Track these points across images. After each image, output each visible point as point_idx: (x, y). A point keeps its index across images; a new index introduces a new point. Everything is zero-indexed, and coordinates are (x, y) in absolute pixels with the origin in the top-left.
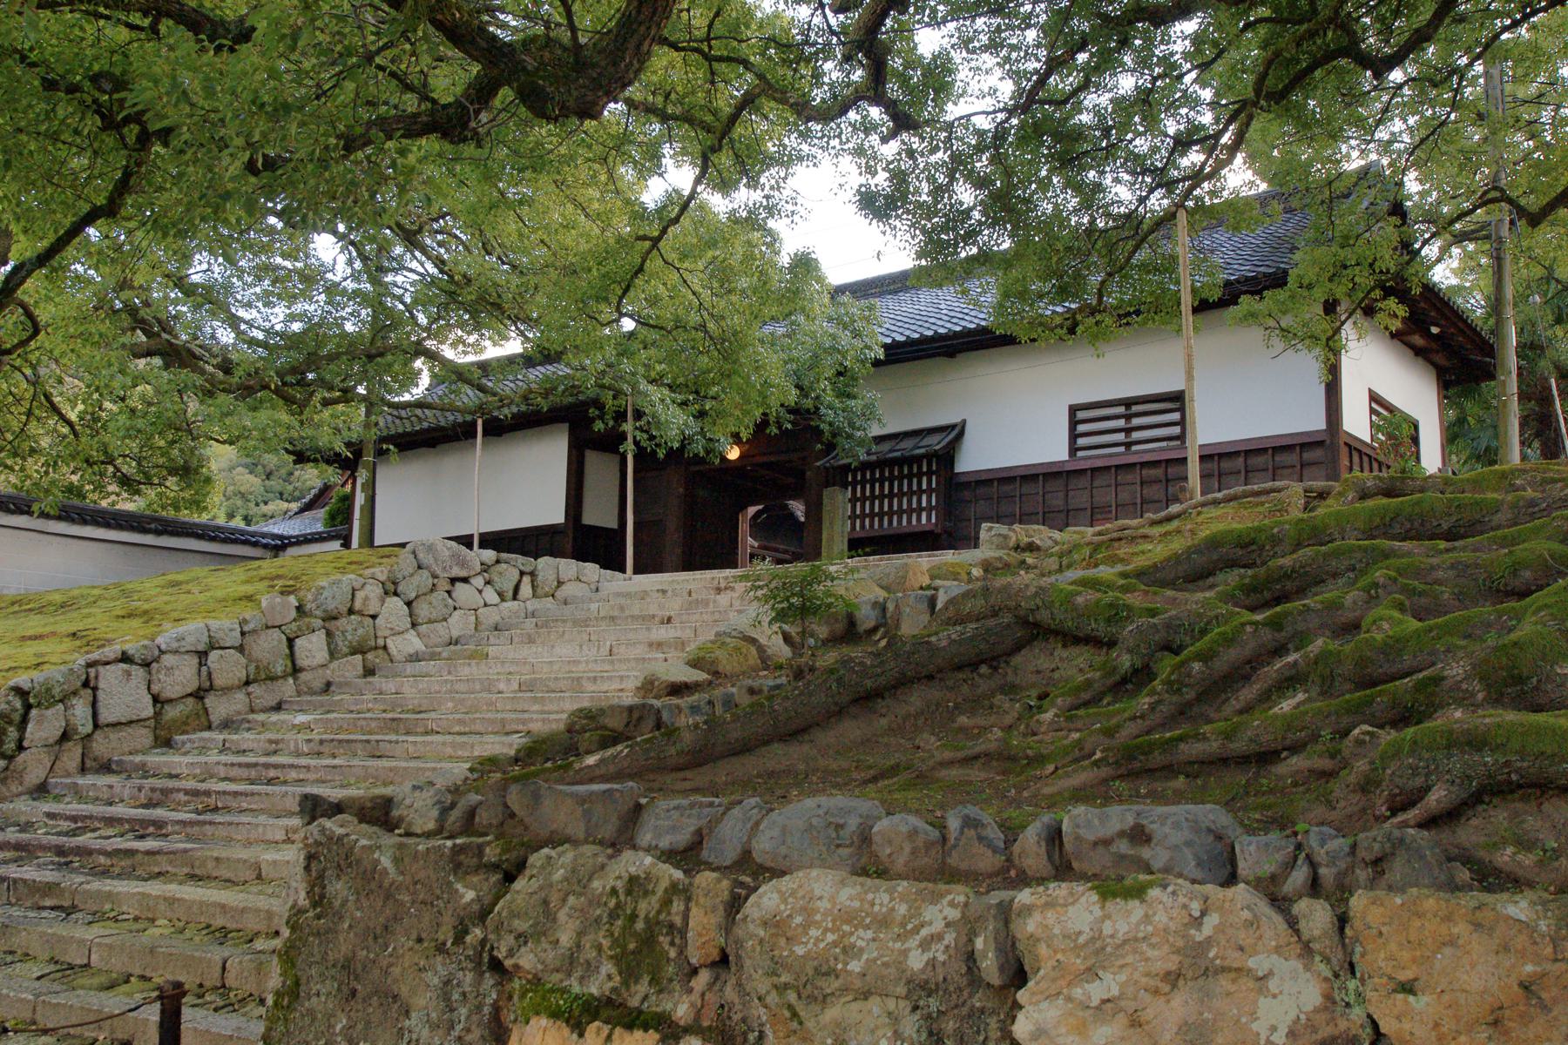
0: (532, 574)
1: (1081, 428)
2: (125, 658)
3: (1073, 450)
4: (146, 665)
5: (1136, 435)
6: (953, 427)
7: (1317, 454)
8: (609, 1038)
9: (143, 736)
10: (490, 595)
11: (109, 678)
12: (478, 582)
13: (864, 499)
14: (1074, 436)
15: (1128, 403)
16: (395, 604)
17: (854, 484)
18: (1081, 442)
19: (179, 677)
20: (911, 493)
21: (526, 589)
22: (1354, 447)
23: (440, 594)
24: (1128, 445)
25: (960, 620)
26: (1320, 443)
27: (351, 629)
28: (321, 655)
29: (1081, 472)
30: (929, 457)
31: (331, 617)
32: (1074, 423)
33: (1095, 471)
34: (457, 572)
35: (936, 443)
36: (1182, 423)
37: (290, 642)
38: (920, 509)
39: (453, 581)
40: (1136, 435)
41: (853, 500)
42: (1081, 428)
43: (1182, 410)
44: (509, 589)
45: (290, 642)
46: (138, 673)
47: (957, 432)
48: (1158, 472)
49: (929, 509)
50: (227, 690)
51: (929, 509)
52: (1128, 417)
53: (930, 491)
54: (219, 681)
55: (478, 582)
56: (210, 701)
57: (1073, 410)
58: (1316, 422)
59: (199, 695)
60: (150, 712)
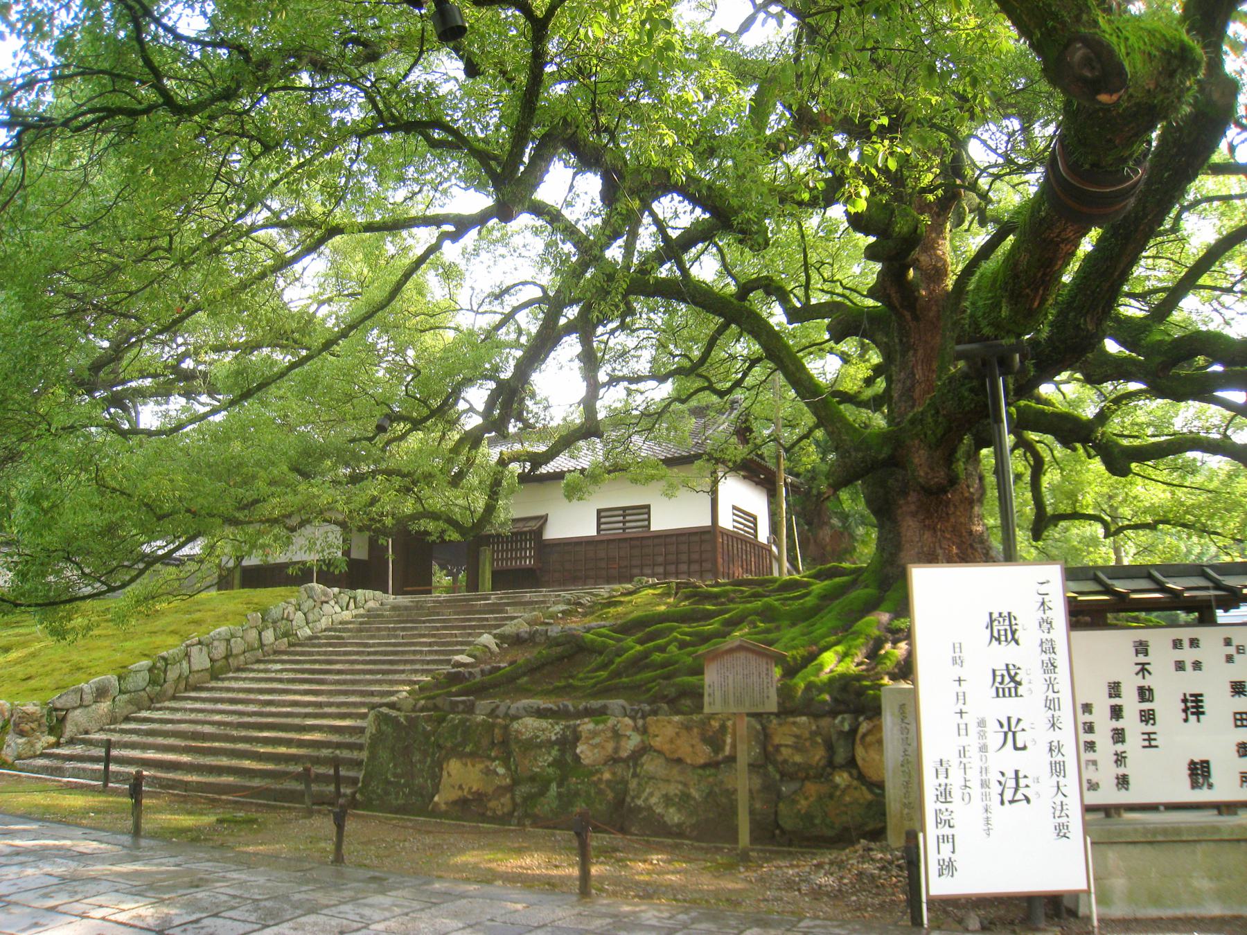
0: (355, 599)
1: (603, 520)
2: (200, 643)
3: (598, 531)
4: (208, 646)
5: (628, 525)
6: (541, 517)
7: (707, 537)
8: (1178, 365)
9: (207, 675)
10: (338, 609)
11: (195, 650)
12: (332, 603)
13: (498, 551)
14: (599, 524)
15: (624, 509)
16: (300, 614)
17: (493, 544)
18: (603, 527)
19: (220, 650)
20: (521, 549)
21: (352, 605)
22: (724, 533)
23: (317, 609)
24: (624, 529)
25: (558, 645)
26: (709, 532)
27: (282, 625)
28: (272, 639)
29: (602, 541)
30: (530, 532)
31: (274, 622)
32: (599, 518)
33: (609, 541)
34: (323, 598)
35: (534, 525)
36: (649, 520)
37: (260, 634)
38: (526, 557)
39: (322, 603)
40: (628, 525)
41: (494, 551)
42: (603, 520)
43: (649, 513)
44: (345, 605)
45: (260, 634)
46: (205, 649)
47: (544, 519)
48: (638, 543)
49: (530, 557)
50: (237, 656)
51: (530, 557)
52: (624, 516)
53: (530, 549)
54: (235, 652)
55: (332, 603)
56: (231, 660)
57: (599, 511)
58: (709, 523)
59: (226, 657)
60: (209, 665)
